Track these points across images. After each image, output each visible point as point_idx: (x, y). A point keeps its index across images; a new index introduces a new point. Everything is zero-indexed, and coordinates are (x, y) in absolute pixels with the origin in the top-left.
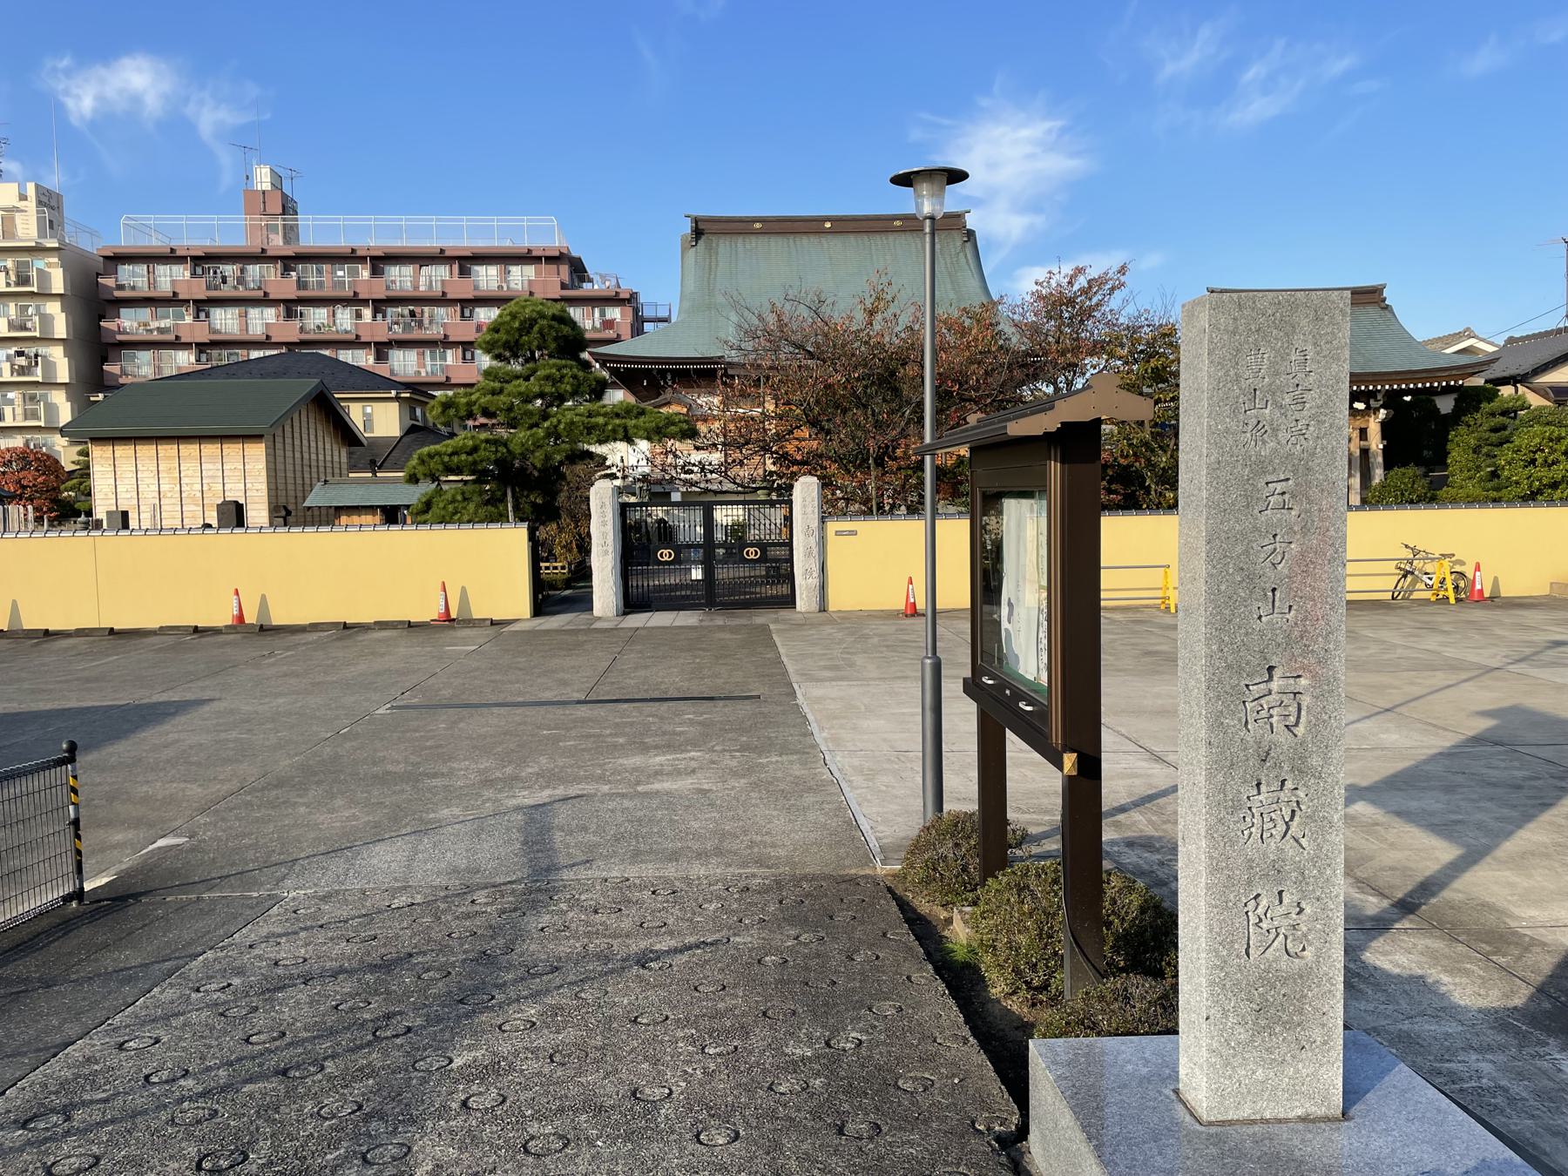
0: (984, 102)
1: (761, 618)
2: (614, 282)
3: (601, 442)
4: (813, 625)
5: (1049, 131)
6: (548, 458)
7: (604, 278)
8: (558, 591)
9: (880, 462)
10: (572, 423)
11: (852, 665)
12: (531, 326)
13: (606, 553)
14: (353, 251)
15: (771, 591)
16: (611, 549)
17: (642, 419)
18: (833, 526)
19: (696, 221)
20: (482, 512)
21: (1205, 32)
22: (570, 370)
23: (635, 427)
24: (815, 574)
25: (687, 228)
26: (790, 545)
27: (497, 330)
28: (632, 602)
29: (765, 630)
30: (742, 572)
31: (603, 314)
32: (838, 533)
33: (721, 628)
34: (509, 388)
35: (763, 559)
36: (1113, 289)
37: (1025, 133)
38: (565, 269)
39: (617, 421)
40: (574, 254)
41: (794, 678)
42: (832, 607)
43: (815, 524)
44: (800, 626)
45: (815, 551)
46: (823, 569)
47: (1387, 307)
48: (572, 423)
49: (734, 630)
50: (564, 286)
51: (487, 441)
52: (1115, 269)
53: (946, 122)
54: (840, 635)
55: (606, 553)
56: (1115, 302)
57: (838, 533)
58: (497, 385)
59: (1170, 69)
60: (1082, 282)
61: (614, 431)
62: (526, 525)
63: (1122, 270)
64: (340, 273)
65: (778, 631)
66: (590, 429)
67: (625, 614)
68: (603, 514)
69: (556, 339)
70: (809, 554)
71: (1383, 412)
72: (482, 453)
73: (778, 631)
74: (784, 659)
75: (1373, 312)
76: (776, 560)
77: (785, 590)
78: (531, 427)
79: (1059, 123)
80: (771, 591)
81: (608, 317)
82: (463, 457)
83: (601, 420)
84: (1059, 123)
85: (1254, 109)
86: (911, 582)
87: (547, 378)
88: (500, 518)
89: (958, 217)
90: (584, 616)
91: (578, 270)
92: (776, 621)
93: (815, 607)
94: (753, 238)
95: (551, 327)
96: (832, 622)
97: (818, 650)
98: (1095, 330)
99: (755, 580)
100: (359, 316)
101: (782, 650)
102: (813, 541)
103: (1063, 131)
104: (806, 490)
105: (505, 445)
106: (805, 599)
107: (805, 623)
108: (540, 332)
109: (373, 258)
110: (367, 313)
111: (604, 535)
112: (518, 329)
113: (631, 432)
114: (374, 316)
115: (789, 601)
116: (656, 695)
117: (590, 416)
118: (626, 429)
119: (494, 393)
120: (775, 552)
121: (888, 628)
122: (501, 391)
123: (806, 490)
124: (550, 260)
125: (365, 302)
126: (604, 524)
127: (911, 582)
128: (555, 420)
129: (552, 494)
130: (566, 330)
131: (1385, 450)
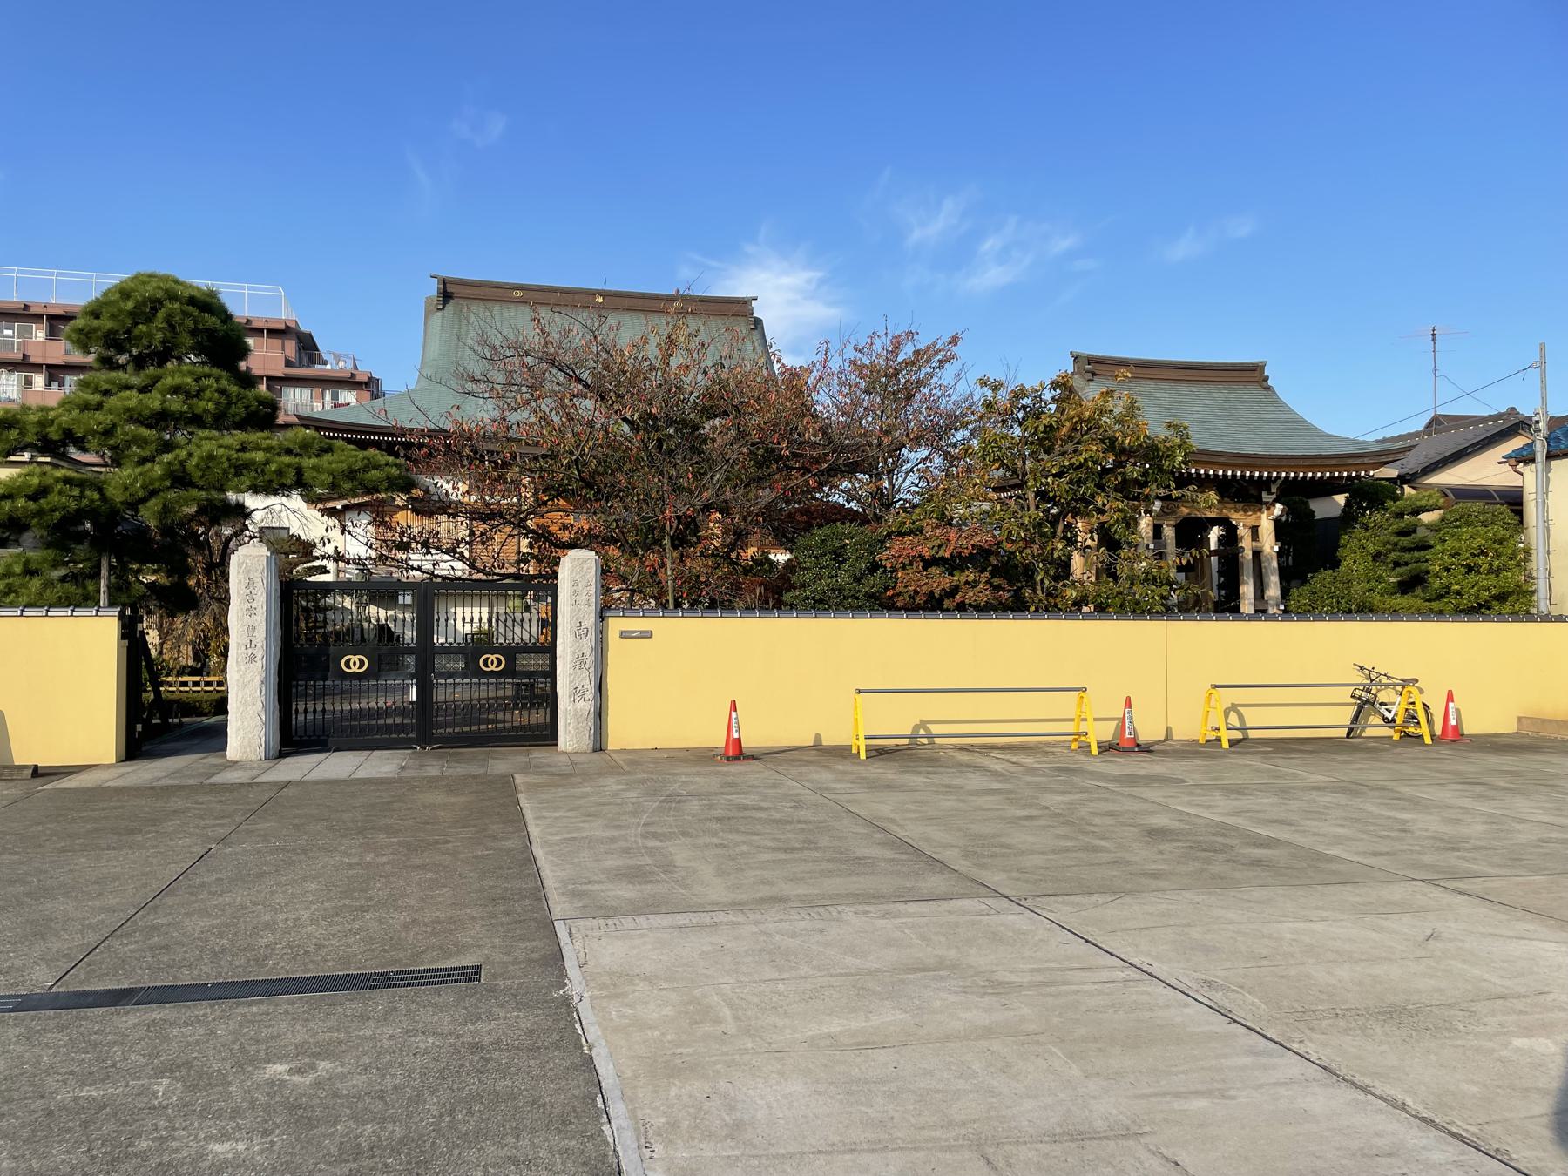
0: (750, 249)
1: (503, 762)
2: (350, 366)
3: (255, 490)
4: (587, 776)
5: (809, 281)
6: (166, 510)
7: (338, 358)
8: (164, 716)
9: (679, 541)
10: (211, 457)
11: (668, 867)
12: (155, 310)
13: (252, 658)
14: (26, 307)
15: (520, 718)
16: (260, 653)
17: (327, 457)
18: (616, 624)
19: (444, 282)
20: (59, 589)
21: (949, 204)
22: (217, 381)
23: (315, 468)
24: (589, 695)
25: (433, 289)
26: (550, 650)
27: (97, 315)
28: (293, 738)
29: (506, 786)
30: (484, 691)
31: (335, 397)
32: (625, 634)
33: (433, 782)
34: (112, 401)
35: (510, 671)
36: (942, 363)
37: (786, 281)
38: (291, 347)
39: (287, 459)
40: (304, 328)
41: (559, 906)
42: (614, 742)
43: (590, 619)
44: (563, 777)
45: (590, 660)
46: (601, 687)
47: (1268, 388)
48: (211, 457)
49: (452, 786)
50: (288, 363)
51: (67, 481)
52: (946, 339)
53: (714, 264)
54: (632, 796)
55: (252, 658)
56: (947, 375)
57: (625, 634)
58: (97, 397)
59: (917, 235)
60: (906, 353)
61: (280, 473)
62: (116, 612)
63: (954, 341)
64: (8, 332)
65: (530, 787)
66: (240, 469)
67: (282, 755)
68: (250, 598)
69: (194, 332)
70: (579, 664)
71: (1279, 506)
72: (54, 499)
73: (530, 787)
74: (538, 852)
75: (1254, 391)
76: (530, 675)
77: (540, 716)
78: (143, 461)
79: (819, 274)
80: (520, 718)
81: (341, 400)
82: (21, 502)
83: (259, 456)
84: (819, 274)
85: (991, 277)
86: (734, 707)
87: (176, 390)
88: (87, 600)
89: (745, 302)
90: (212, 759)
91: (307, 347)
92: (526, 769)
93: (586, 743)
94: (512, 307)
95: (185, 314)
96: (614, 770)
97: (597, 829)
98: (917, 414)
99: (514, 703)
100: (28, 383)
101: (534, 831)
102: (587, 646)
103: (822, 282)
104: (577, 572)
105: (100, 490)
106: (572, 733)
107: (571, 774)
108: (169, 320)
109: (51, 317)
110: (39, 380)
111: (251, 630)
112: (131, 314)
113: (307, 475)
114: (48, 385)
115: (547, 735)
116: (231, 971)
117: (243, 449)
118: (299, 471)
119: (85, 407)
120: (525, 662)
121: (706, 780)
122: (99, 407)
123: (577, 572)
124: (273, 333)
125: (37, 367)
126: (251, 612)
127: (734, 707)
128: (183, 454)
129: (180, 569)
130: (212, 321)
131: (1279, 554)
